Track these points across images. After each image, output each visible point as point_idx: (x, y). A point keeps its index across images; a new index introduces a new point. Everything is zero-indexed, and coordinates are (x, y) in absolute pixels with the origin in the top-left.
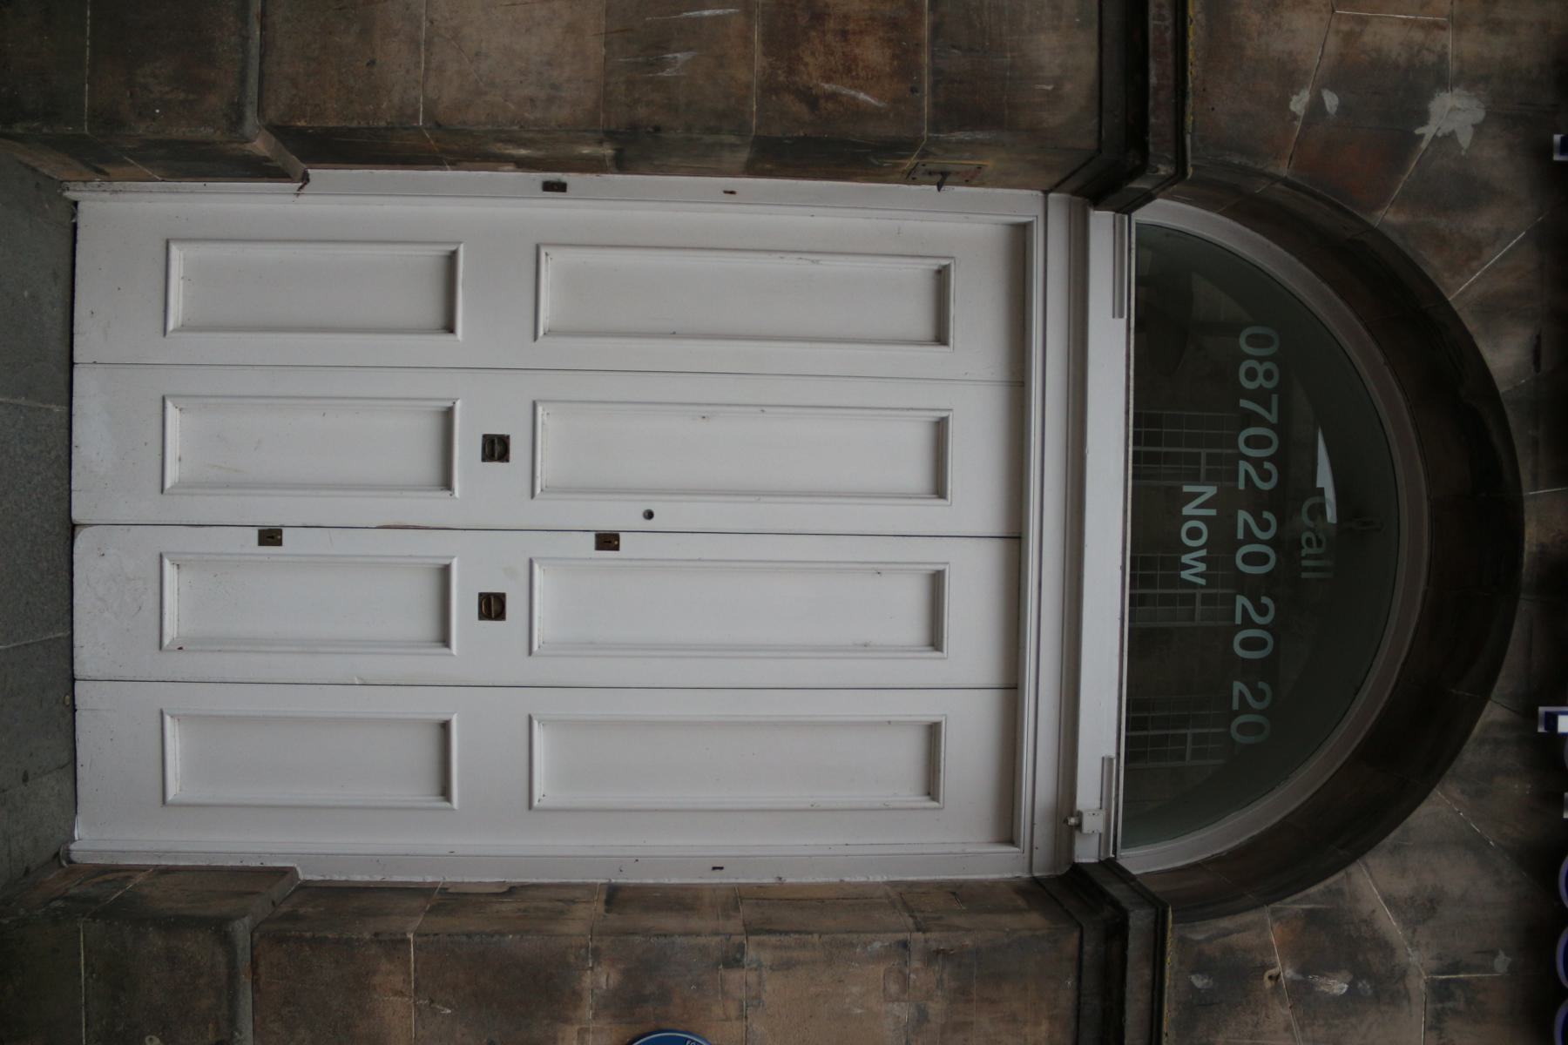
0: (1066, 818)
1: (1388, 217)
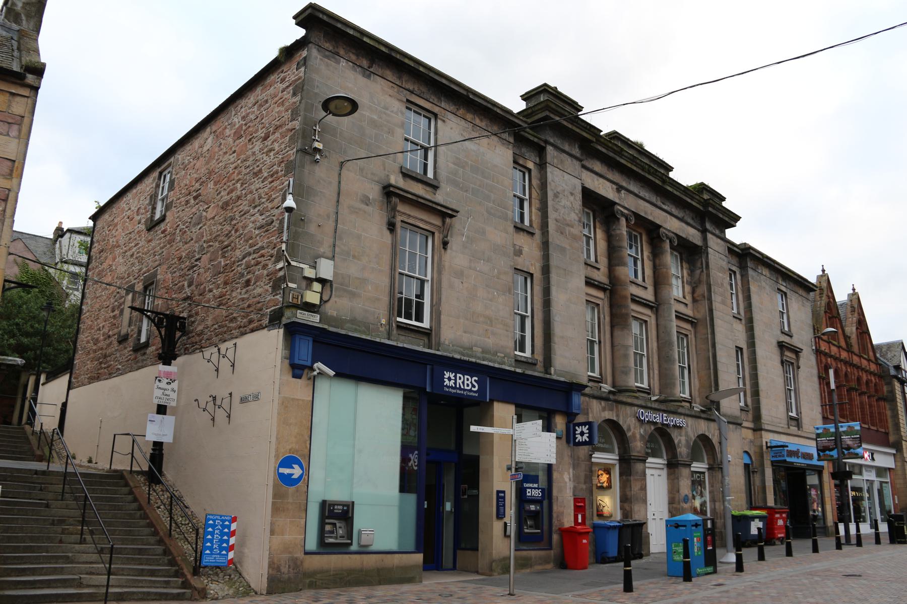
0: (664, 464)
1: (647, 437)
